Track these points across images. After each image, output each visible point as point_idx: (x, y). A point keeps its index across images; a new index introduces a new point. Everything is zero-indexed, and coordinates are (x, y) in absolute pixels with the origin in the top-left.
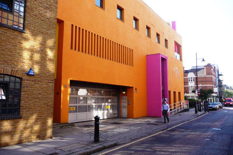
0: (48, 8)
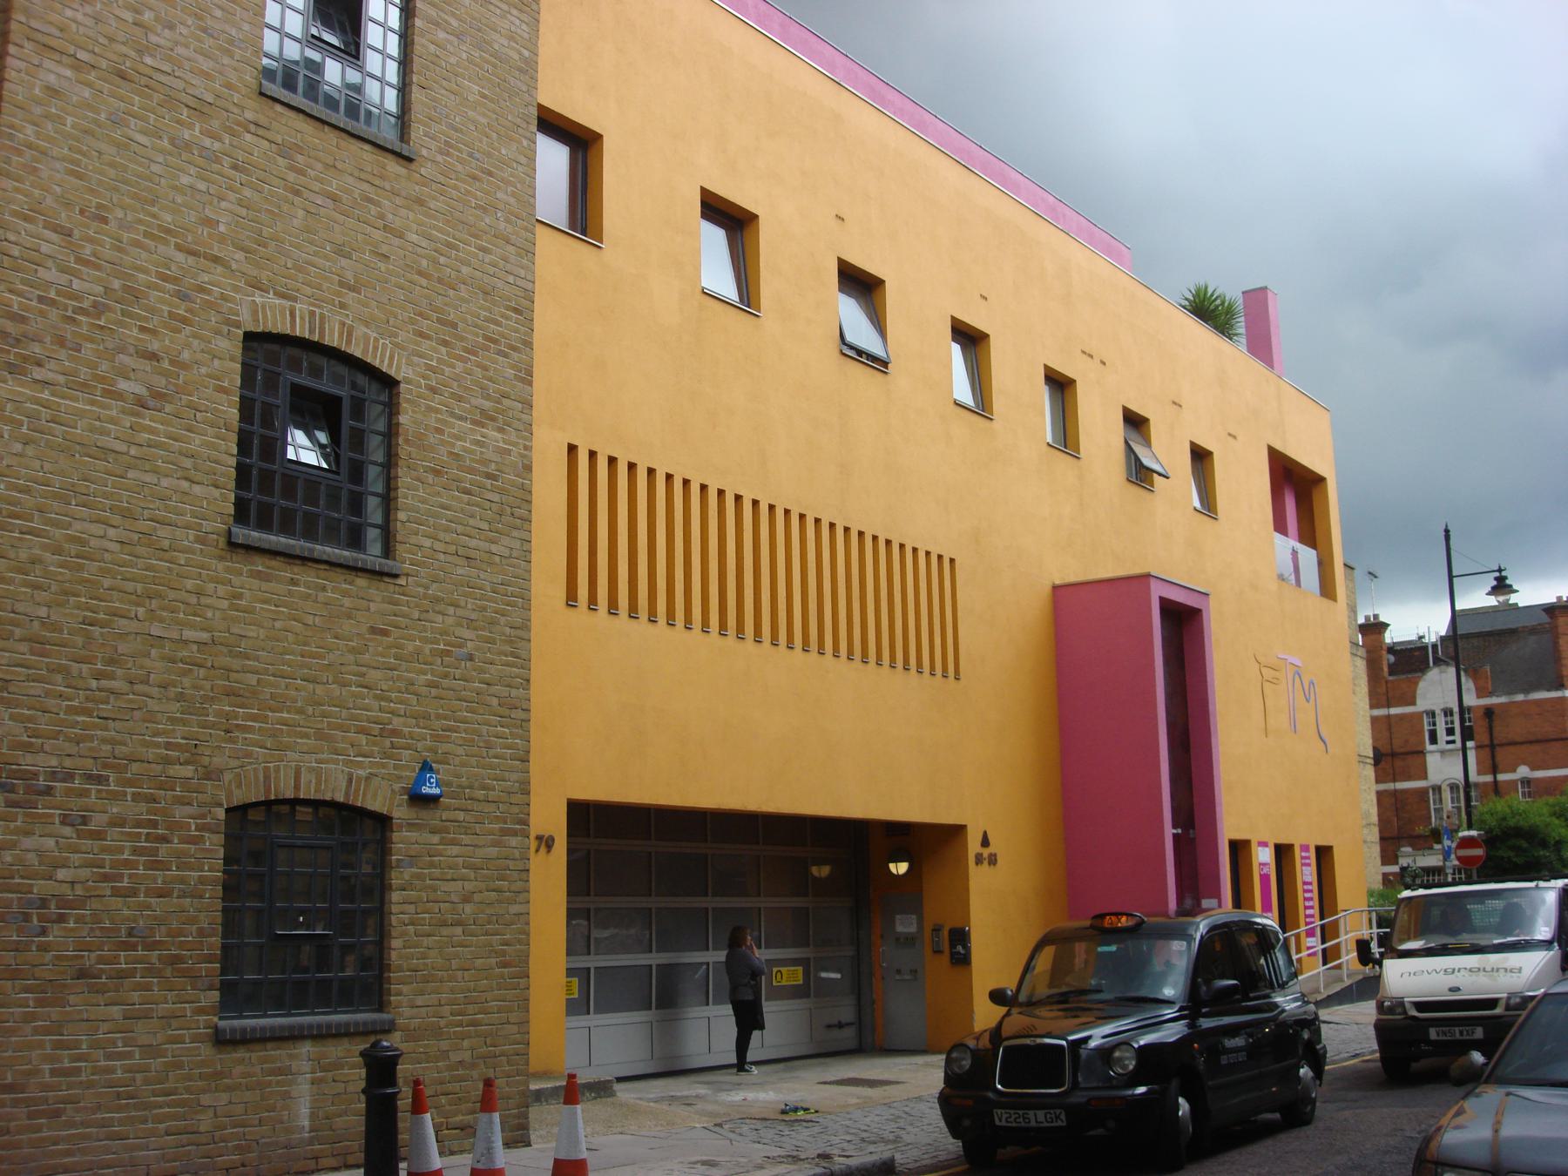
0: (493, 419)
